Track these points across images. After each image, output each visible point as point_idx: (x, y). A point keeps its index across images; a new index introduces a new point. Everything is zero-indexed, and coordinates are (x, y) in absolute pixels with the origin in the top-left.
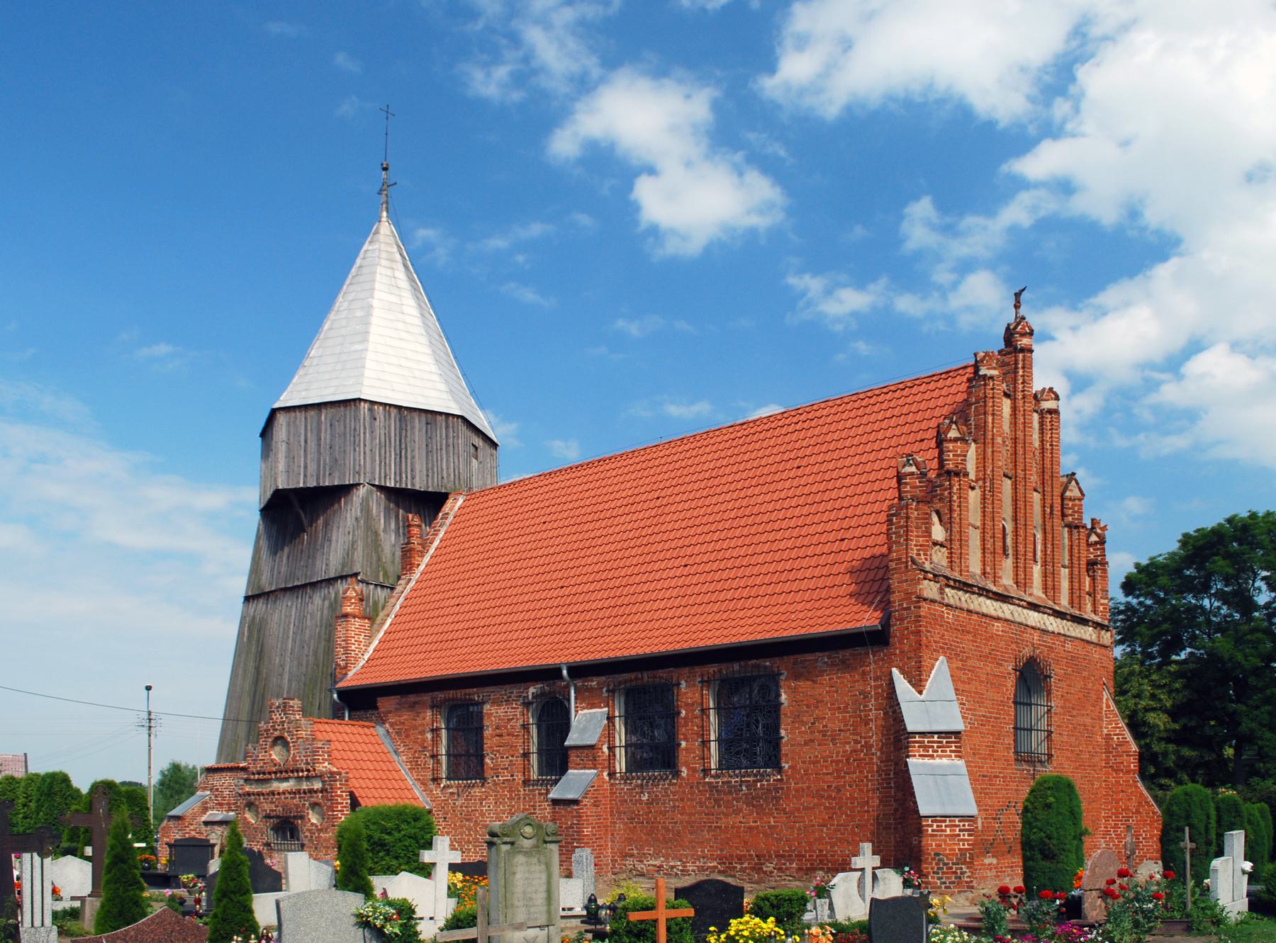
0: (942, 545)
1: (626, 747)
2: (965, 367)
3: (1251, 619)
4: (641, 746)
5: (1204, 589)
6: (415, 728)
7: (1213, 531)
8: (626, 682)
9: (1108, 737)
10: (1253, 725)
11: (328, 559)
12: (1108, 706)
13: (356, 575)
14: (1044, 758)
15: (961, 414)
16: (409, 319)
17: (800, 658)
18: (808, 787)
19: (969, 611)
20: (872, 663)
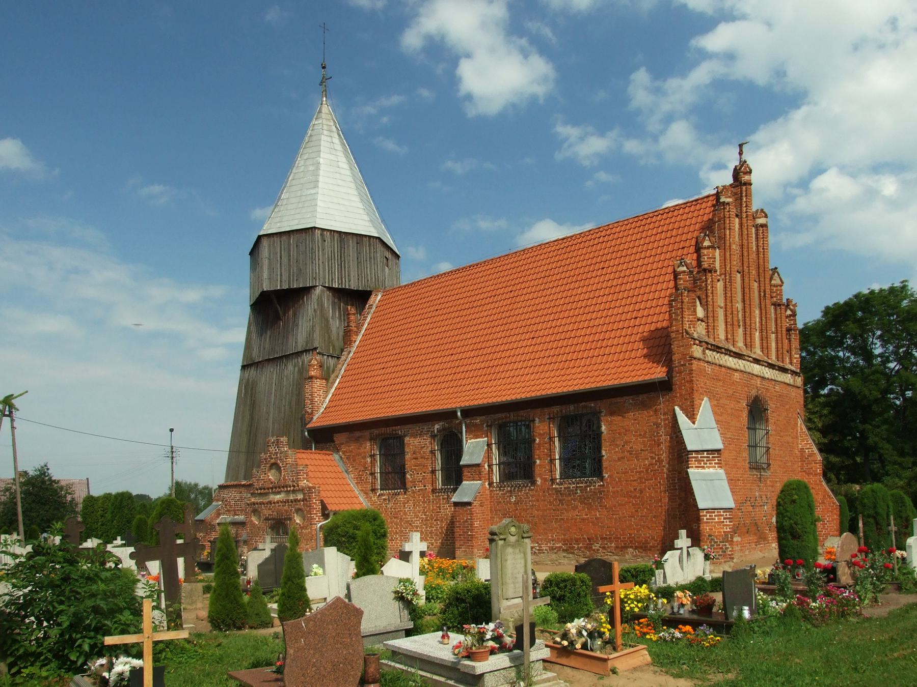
0: (702, 321)
1: (499, 465)
2: (708, 197)
3: (873, 365)
4: (509, 464)
5: (841, 344)
6: (359, 454)
7: (846, 303)
8: (499, 419)
9: (802, 451)
10: (877, 439)
11: (296, 339)
12: (801, 429)
13: (316, 349)
14: (765, 466)
15: (708, 228)
16: (342, 171)
17: (614, 400)
18: (622, 490)
19: (720, 366)
20: (662, 403)
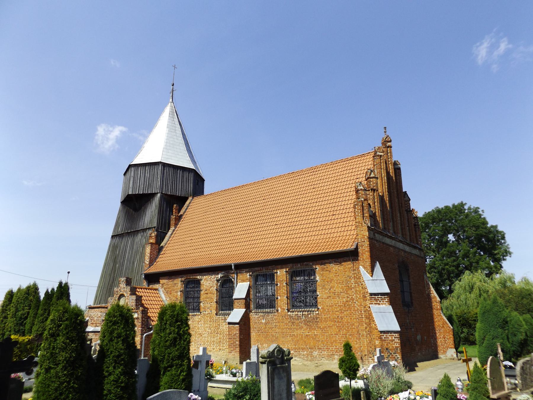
18: (330, 317)
19: (383, 243)
